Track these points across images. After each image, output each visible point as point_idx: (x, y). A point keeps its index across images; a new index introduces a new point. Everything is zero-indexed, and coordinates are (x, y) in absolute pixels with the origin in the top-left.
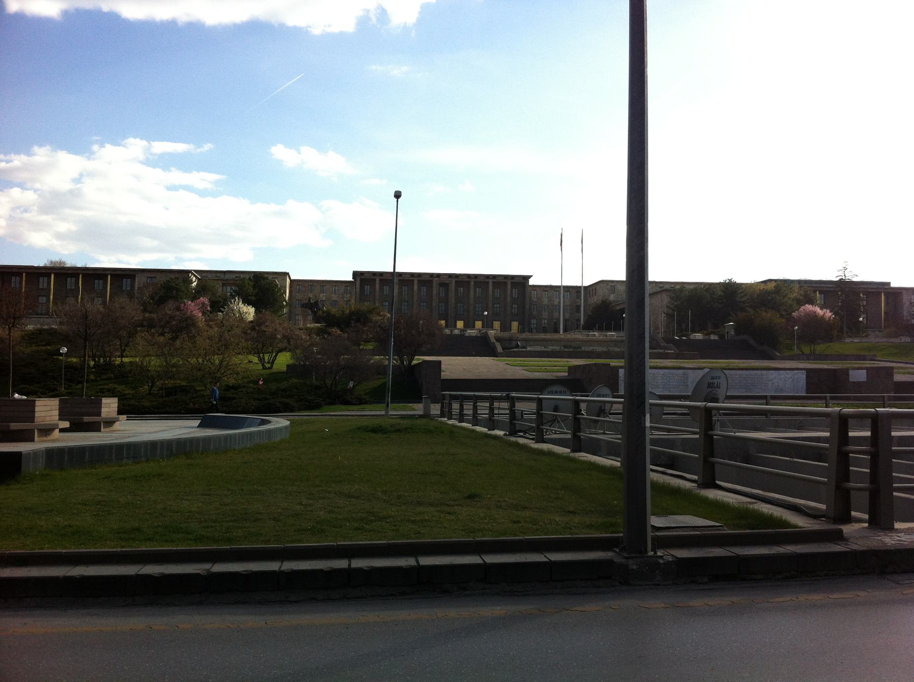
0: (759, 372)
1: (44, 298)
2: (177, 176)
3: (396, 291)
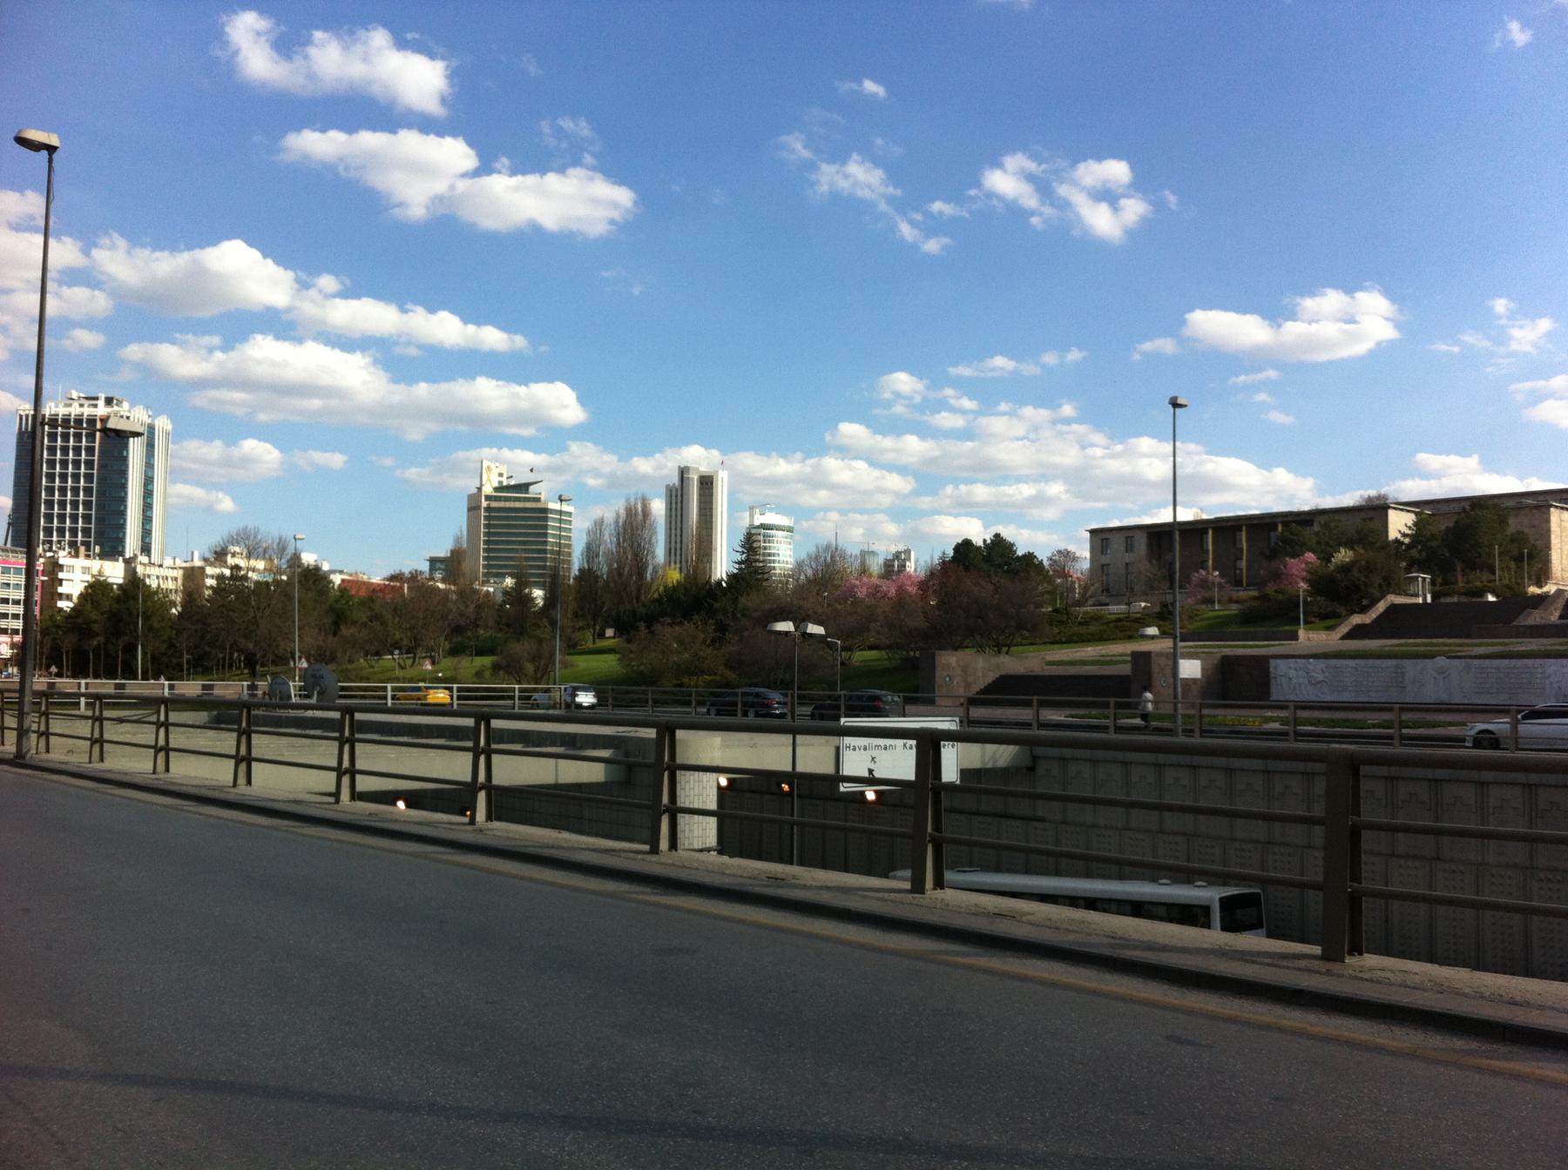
0: (1529, 662)
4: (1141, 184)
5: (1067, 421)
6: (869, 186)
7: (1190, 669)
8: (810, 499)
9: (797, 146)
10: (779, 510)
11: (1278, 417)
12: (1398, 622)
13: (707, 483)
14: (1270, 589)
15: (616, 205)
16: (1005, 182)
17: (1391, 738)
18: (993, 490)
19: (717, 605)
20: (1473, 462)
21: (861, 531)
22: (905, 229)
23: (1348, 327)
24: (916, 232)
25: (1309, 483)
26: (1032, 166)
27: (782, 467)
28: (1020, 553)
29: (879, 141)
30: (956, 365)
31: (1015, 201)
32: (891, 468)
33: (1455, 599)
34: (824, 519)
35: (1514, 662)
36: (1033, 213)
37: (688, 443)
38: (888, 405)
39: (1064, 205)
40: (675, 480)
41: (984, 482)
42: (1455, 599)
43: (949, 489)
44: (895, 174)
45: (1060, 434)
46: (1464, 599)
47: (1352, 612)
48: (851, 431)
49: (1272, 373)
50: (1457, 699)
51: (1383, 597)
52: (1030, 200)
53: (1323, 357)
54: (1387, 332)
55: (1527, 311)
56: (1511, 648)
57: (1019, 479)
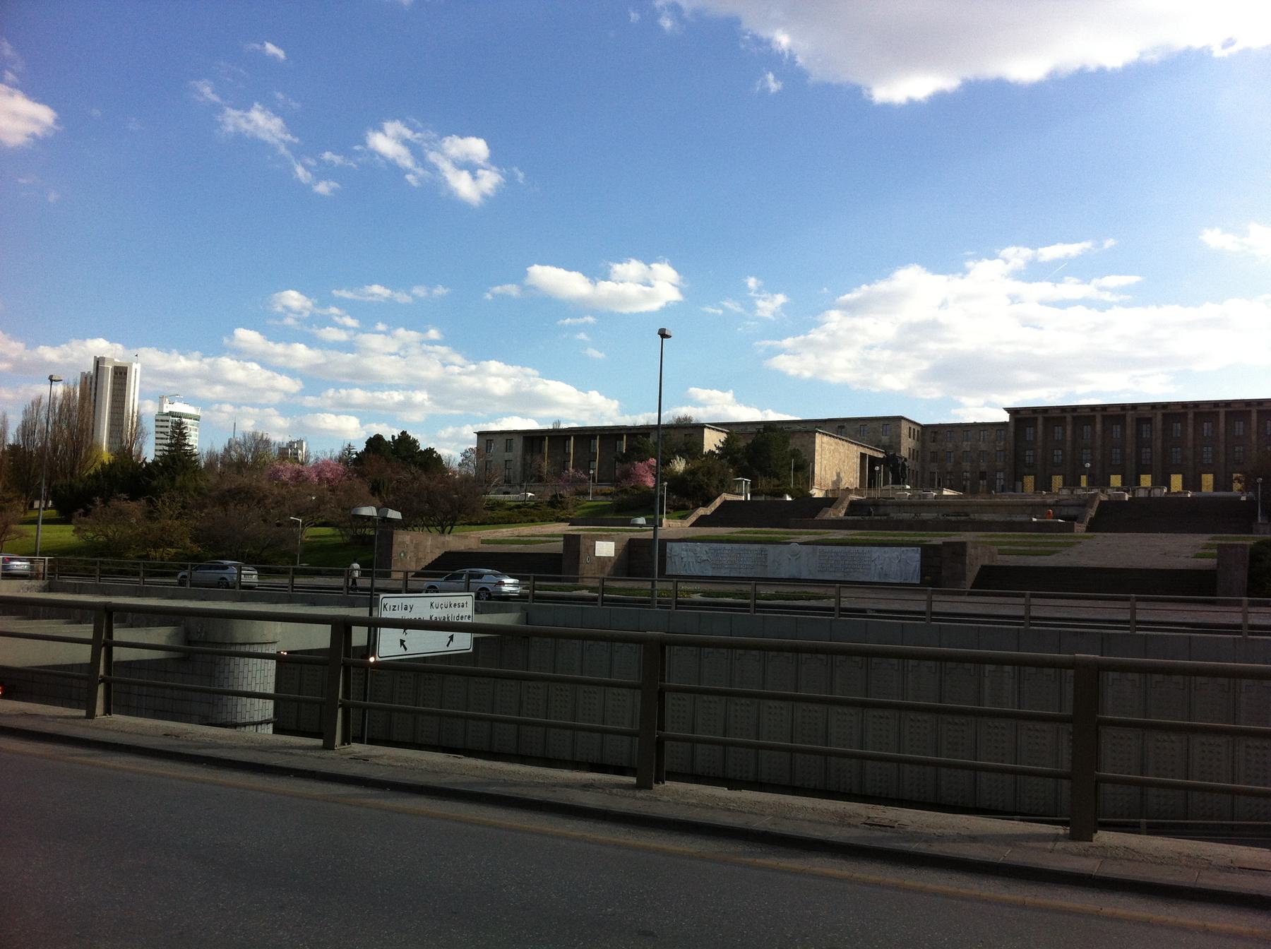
0: (860, 549)
1: (1031, 453)
2: (1071, 288)
3: (1069, 432)
4: (497, 159)
5: (433, 343)
6: (270, 131)
7: (606, 549)
8: (205, 392)
9: (207, 91)
10: (187, 402)
11: (593, 353)
12: (728, 515)
13: (121, 374)
14: (626, 485)
15: (36, 121)
16: (386, 142)
17: (747, 605)
18: (369, 394)
19: (155, 483)
20: (729, 396)
21: (252, 422)
22: (300, 171)
23: (647, 289)
24: (309, 175)
25: (615, 404)
26: (408, 133)
27: (182, 363)
28: (423, 448)
29: (280, 96)
30: (339, 288)
31: (394, 160)
32: (280, 370)
33: (763, 498)
34: (219, 411)
35: (848, 548)
36: (408, 171)
37: (94, 336)
38: (280, 317)
39: (434, 169)
40: (90, 368)
41: (362, 388)
42: (763, 498)
43: (331, 392)
44: (292, 123)
45: (425, 352)
46: (769, 499)
47: (698, 507)
48: (247, 336)
49: (590, 319)
50: (805, 576)
51: (719, 495)
52: (407, 161)
53: (626, 310)
54: (673, 295)
55: (771, 288)
56: (825, 537)
57: (392, 387)
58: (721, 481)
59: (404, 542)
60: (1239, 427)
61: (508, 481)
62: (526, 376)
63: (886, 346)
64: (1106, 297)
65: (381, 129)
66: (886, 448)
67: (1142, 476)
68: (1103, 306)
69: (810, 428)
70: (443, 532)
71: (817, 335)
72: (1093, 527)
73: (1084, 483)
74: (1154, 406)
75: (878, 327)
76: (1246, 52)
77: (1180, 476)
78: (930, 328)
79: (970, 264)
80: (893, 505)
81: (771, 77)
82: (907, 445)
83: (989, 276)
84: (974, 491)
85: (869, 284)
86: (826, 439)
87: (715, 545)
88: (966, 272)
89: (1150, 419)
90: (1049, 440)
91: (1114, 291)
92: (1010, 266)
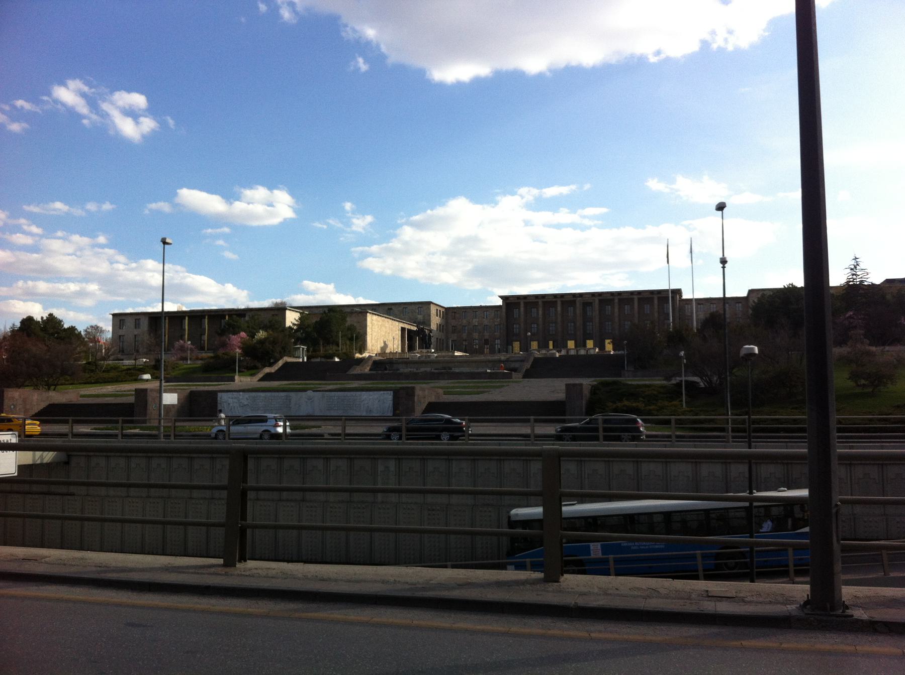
2: (564, 216)
4: (152, 110)
5: (102, 246)
11: (229, 255)
12: (288, 372)
14: (221, 352)
16: (67, 94)
20: (331, 287)
25: (245, 293)
26: (86, 89)
28: (66, 326)
33: (318, 360)
36: (84, 117)
39: (105, 115)
42: (318, 360)
43: (20, 283)
46: (323, 360)
49: (226, 230)
51: (281, 358)
52: (82, 108)
55: (361, 211)
57: (69, 280)
58: (283, 348)
59: (13, 398)
60: (647, 308)
61: (122, 351)
62: (177, 272)
63: (444, 253)
64: (587, 222)
65: (64, 84)
66: (418, 324)
67: (588, 341)
68: (584, 228)
69: (361, 311)
70: (49, 389)
71: (396, 244)
72: (528, 375)
73: (551, 347)
74: (593, 295)
75: (437, 239)
76: (668, 59)
77: (573, 342)
78: (473, 241)
79: (499, 198)
80: (402, 363)
81: (361, 60)
82: (435, 321)
83: (511, 206)
84: (481, 351)
85: (432, 210)
86: (375, 317)
87: (254, 394)
88: (496, 203)
89: (591, 303)
90: (526, 315)
91: (592, 218)
92: (524, 200)
